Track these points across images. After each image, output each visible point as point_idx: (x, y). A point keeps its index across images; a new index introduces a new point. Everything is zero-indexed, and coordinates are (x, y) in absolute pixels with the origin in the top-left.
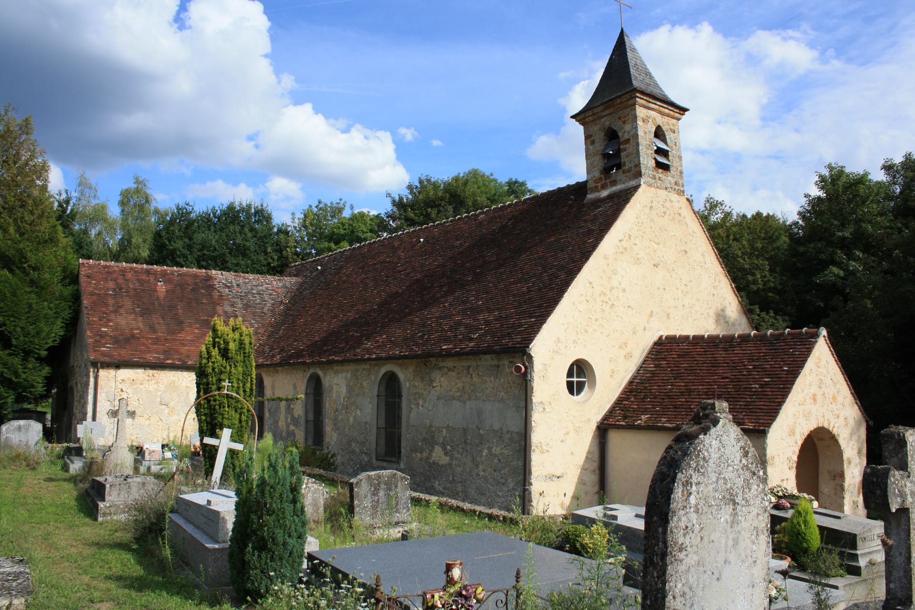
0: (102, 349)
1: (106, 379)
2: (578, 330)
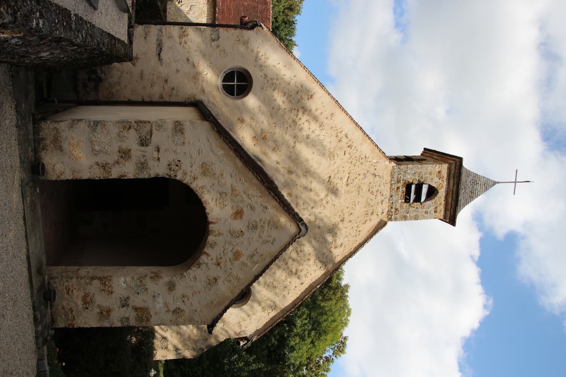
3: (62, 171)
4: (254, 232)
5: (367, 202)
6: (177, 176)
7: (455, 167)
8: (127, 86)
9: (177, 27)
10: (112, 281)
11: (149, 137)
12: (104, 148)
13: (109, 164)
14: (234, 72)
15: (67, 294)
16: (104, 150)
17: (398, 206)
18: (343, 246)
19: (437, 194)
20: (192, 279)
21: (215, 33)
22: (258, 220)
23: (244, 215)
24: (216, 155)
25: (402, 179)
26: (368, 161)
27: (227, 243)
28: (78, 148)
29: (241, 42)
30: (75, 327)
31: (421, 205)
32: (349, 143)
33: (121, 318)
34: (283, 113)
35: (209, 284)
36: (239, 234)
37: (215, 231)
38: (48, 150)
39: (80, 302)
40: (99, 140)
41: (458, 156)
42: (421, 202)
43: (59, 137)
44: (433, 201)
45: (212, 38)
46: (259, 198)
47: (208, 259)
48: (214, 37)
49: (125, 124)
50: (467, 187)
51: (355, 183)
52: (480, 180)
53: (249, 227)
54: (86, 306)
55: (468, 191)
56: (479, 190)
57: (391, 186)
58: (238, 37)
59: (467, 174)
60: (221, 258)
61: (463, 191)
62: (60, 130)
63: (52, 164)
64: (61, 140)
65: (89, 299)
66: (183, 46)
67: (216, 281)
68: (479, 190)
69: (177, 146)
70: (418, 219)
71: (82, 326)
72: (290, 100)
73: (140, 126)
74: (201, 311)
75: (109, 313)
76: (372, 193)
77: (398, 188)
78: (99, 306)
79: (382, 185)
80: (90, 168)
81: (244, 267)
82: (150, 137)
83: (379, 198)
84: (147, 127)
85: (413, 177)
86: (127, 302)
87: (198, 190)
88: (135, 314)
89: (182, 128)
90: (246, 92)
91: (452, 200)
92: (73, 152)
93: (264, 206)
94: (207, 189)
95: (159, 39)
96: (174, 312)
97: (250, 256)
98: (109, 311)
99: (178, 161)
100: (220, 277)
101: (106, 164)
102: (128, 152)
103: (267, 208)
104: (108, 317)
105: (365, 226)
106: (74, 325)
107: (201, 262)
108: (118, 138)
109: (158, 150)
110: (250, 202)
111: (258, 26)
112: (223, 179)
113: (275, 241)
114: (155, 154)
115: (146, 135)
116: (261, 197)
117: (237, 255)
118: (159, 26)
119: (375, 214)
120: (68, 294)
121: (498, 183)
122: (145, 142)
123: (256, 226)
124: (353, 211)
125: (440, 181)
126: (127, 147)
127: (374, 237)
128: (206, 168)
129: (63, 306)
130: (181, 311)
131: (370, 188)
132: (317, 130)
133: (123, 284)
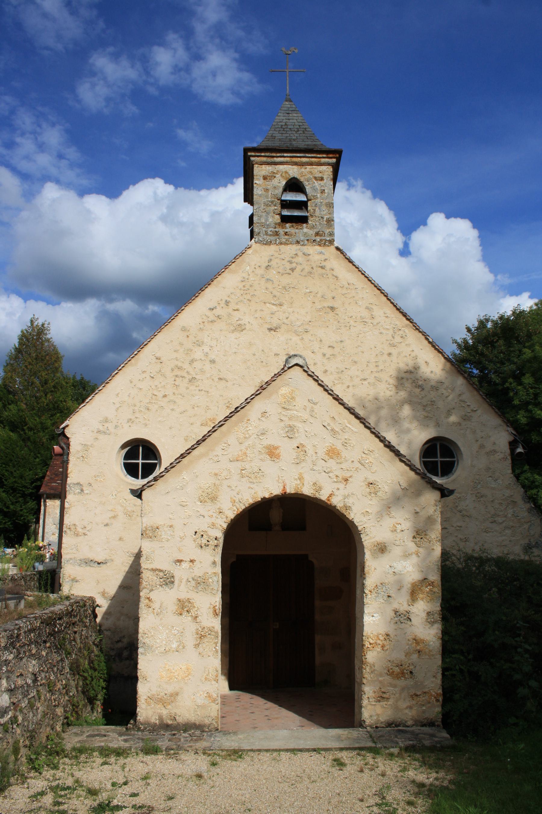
0: (53, 484)
1: (53, 507)
2: (136, 408)
3: (205, 695)
5: (305, 276)
7: (258, 156)
9: (64, 540)
10: (369, 634)
11: (161, 574)
14: (125, 464)
15: (388, 701)
16: (178, 636)
17: (312, 232)
18: (370, 306)
21: (73, 489)
22: (282, 424)
23: (273, 444)
25: (273, 230)
26: (247, 277)
27: (314, 468)
29: (85, 454)
30: (442, 693)
31: (311, 200)
32: (223, 304)
33: (428, 623)
34: (180, 396)
38: (175, 713)
40: (164, 642)
41: (243, 154)
43: (159, 697)
44: (306, 183)
45: (79, 493)
48: (78, 490)
50: (289, 137)
51: (278, 294)
52: (281, 120)
55: (294, 136)
56: (295, 121)
57: (284, 244)
58: (78, 458)
59: (270, 140)
60: (337, 476)
61: (294, 143)
62: (149, 695)
63: (195, 708)
64: (163, 694)
65: (397, 670)
66: (88, 531)
67: (371, 484)
68: (295, 121)
69: (174, 535)
70: (331, 203)
72: (162, 387)
73: (146, 585)
76: (293, 270)
77: (286, 234)
79: (282, 256)
80: (203, 656)
84: (147, 576)
85: (272, 214)
89: (149, 528)
90: (152, 448)
93: (262, 416)
94: (236, 495)
95: (79, 563)
97: (334, 435)
99: (195, 535)
101: (197, 634)
104: (426, 642)
105: (340, 276)
106: (437, 694)
107: (342, 505)
109: (180, 561)
112: (221, 473)
113: (312, 400)
114: (184, 565)
115: (159, 577)
117: (333, 453)
119: (323, 264)
120: (388, 698)
123: (290, 427)
124: (319, 295)
125: (277, 176)
126: (174, 603)
128: (206, 497)
129: (407, 708)
131: (286, 272)
132: (203, 350)
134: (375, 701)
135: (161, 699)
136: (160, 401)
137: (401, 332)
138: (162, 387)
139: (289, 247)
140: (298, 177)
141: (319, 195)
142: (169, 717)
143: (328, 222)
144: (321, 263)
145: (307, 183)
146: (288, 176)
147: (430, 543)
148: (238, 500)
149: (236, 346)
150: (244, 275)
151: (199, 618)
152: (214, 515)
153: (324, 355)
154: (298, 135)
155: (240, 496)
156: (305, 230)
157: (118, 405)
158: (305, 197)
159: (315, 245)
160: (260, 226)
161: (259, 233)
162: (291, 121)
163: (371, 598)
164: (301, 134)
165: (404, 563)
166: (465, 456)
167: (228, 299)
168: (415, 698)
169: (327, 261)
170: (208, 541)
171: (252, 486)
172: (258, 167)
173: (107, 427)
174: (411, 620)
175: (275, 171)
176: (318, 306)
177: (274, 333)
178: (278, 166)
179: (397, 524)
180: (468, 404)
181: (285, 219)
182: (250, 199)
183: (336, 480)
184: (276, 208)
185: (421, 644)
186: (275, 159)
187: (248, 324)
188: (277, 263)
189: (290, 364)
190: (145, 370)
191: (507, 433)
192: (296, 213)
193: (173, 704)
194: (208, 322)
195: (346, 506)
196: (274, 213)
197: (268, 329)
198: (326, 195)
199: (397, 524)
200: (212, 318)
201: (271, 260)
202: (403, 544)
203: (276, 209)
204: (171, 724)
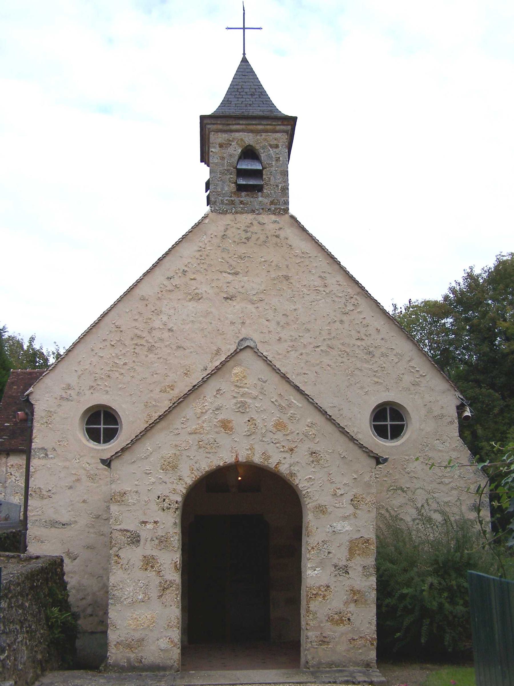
4: (249, 406)
6: (177, 501)
7: (214, 124)
8: (103, 567)
9: (30, 502)
11: (129, 534)
12: (142, 588)
13: (160, 582)
18: (323, 275)
19: (252, 146)
20: (311, 484)
21: (38, 453)
22: (234, 401)
24: (151, 453)
25: (229, 199)
26: (203, 246)
28: (140, 619)
35: (318, 461)
36: (252, 424)
37: (247, 454)
38: (142, 656)
39: (342, 628)
42: (261, 168)
43: (127, 642)
46: (206, 400)
47: (284, 464)
48: (42, 455)
49: (113, 561)
51: (234, 263)
52: (237, 84)
53: (243, 411)
54: (345, 620)
56: (252, 84)
58: (42, 424)
59: (227, 105)
60: (283, 446)
62: (118, 641)
64: (130, 640)
66: (53, 493)
67: (314, 453)
71: (374, 628)
72: (121, 355)
73: (115, 544)
74: (356, 472)
75: (356, 591)
76: (248, 239)
77: (241, 202)
78: (346, 603)
79: (238, 226)
81: (296, 417)
82: (129, 533)
83: (256, 228)
84: (117, 536)
86: (341, 568)
87: (194, 474)
88: (358, 557)
91: (259, 124)
92: (145, 626)
93: (217, 394)
96: (355, 507)
98: (354, 592)
99: (158, 499)
100: (309, 448)
102: (147, 558)
103: (219, 390)
104: (362, 593)
106: (372, 638)
107: (288, 472)
108: (129, 572)
109: (145, 523)
110: (211, 411)
111: (28, 398)
113: (262, 379)
114: (150, 526)
115: (126, 537)
116: (205, 397)
117: (280, 426)
118: (28, 525)
120: (328, 642)
121: (244, 54)
122: (135, 538)
123: (242, 403)
125: (233, 144)
127: (310, 232)
130: (356, 498)
131: (241, 241)
133: (316, 571)
134: (317, 644)
135: (129, 644)
136: (120, 368)
137: (353, 300)
138: (121, 355)
139: (244, 216)
140: (253, 145)
141: (274, 163)
142: (136, 660)
143: (283, 191)
144: (275, 232)
145: (262, 151)
146: (243, 144)
147: (366, 505)
148: (196, 469)
149: (193, 315)
150: (201, 244)
151: (162, 572)
152: (175, 481)
153: (278, 323)
154: (254, 100)
155: (197, 465)
156: (260, 199)
157: (80, 373)
158: (261, 165)
159: (269, 214)
160: (216, 195)
161: (215, 202)
162: (247, 84)
163: (314, 554)
164: (256, 98)
165: (343, 523)
166: (413, 420)
167: (186, 269)
168: (352, 642)
169: (281, 230)
170: (170, 505)
171: (208, 455)
172: (214, 135)
173: (70, 394)
174: (349, 573)
175: (231, 139)
176: (273, 275)
177: (230, 302)
178: (234, 133)
179: (337, 488)
180: (417, 369)
181: (240, 188)
182: (207, 160)
183: (283, 450)
184: (232, 176)
185: (357, 595)
186: (231, 126)
187: (204, 293)
188: (233, 233)
189: (242, 346)
190: (106, 338)
191: (454, 397)
192: (252, 182)
193: (140, 649)
194: (166, 291)
195: (291, 473)
196: (230, 182)
197: (224, 298)
198: (281, 162)
199: (337, 488)
200: (170, 287)
201: (227, 229)
202: (342, 506)
203: (231, 178)
204: (138, 666)
